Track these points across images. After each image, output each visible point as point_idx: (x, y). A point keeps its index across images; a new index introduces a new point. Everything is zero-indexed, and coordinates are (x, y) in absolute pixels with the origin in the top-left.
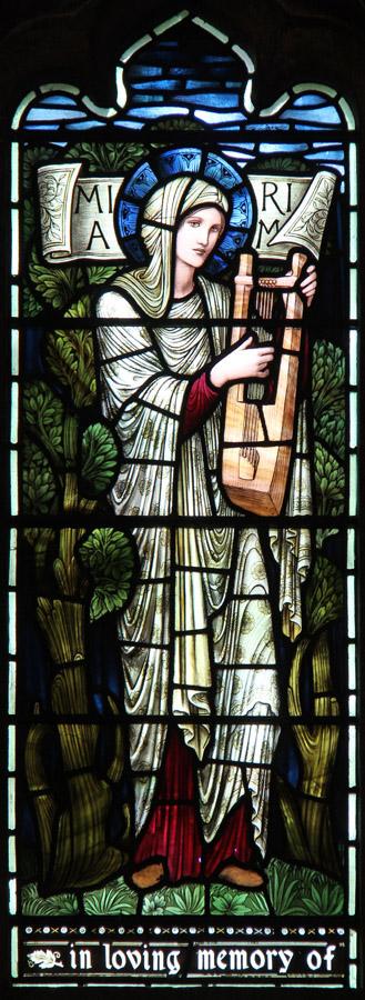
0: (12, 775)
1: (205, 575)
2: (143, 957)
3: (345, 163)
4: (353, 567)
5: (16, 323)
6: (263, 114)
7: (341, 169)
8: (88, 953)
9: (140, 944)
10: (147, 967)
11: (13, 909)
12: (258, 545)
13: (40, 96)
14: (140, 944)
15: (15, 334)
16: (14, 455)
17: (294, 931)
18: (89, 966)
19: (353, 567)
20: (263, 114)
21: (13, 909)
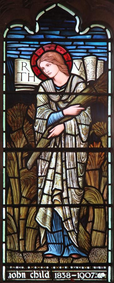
0: (4, 132)
1: (52, 242)
2: (39, 275)
3: (107, 57)
4: (110, 147)
5: (4, 93)
6: (81, 33)
7: (106, 59)
8: (24, 273)
9: (38, 271)
10: (41, 277)
11: (4, 203)
12: (87, 76)
13: (10, 29)
14: (38, 271)
15: (4, 95)
16: (4, 113)
17: (86, 268)
18: (25, 277)
19: (110, 147)
20: (81, 33)
21: (4, 203)
